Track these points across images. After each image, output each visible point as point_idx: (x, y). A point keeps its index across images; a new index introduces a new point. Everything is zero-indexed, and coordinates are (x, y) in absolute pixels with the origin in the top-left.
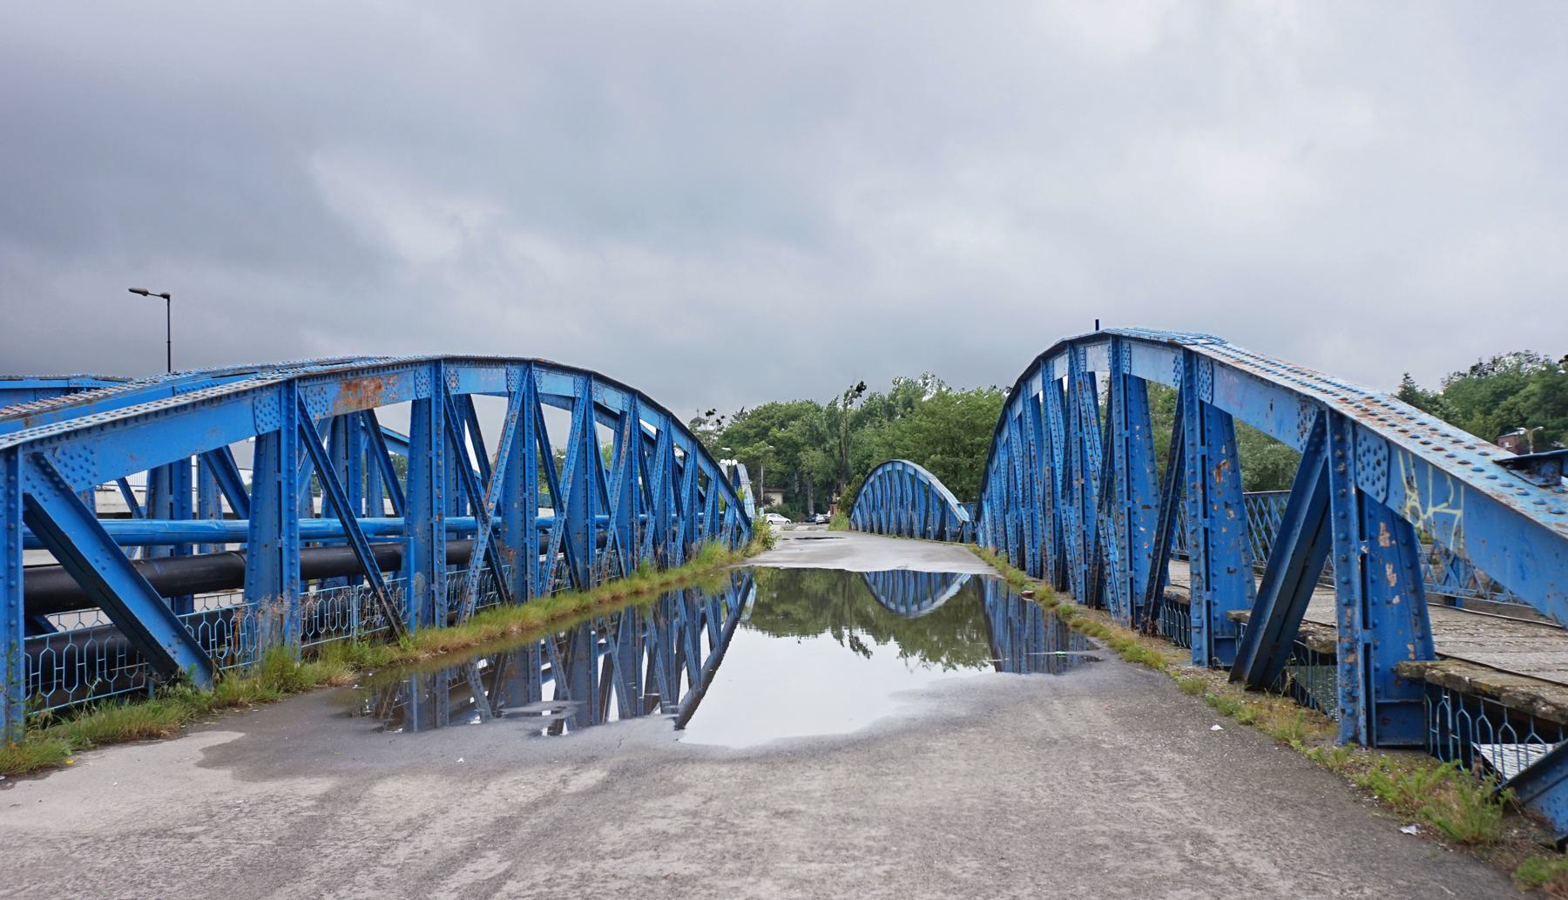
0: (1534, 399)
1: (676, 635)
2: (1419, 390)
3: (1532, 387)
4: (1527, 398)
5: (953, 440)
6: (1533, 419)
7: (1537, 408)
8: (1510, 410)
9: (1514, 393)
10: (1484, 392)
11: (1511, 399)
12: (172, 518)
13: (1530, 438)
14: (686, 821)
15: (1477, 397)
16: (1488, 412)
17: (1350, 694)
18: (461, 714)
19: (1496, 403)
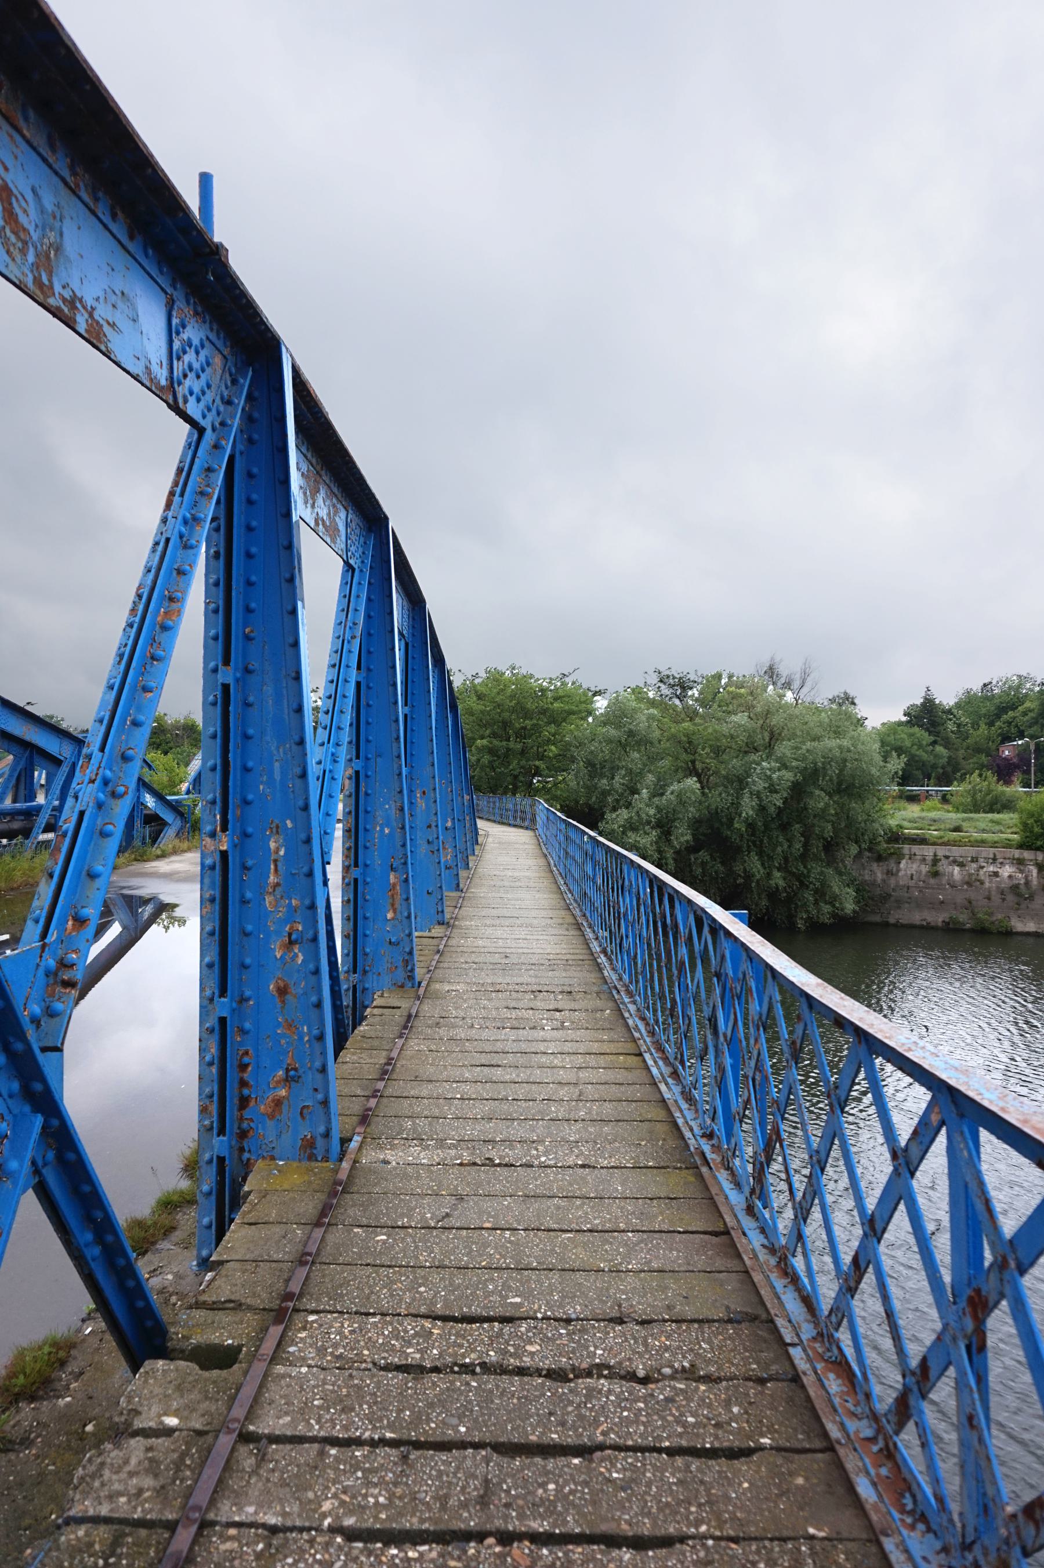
0: (1031, 715)
1: (751, 1083)
2: (937, 702)
3: (1028, 704)
4: (1025, 714)
5: (506, 724)
6: (1031, 731)
7: (1035, 722)
8: (1010, 723)
9: (1014, 708)
10: (990, 707)
11: (1011, 714)
12: (26, 802)
13: (1032, 747)
14: (418, 979)
15: (984, 711)
16: (991, 724)
17: (335, 761)
18: (130, 614)
19: (998, 716)
